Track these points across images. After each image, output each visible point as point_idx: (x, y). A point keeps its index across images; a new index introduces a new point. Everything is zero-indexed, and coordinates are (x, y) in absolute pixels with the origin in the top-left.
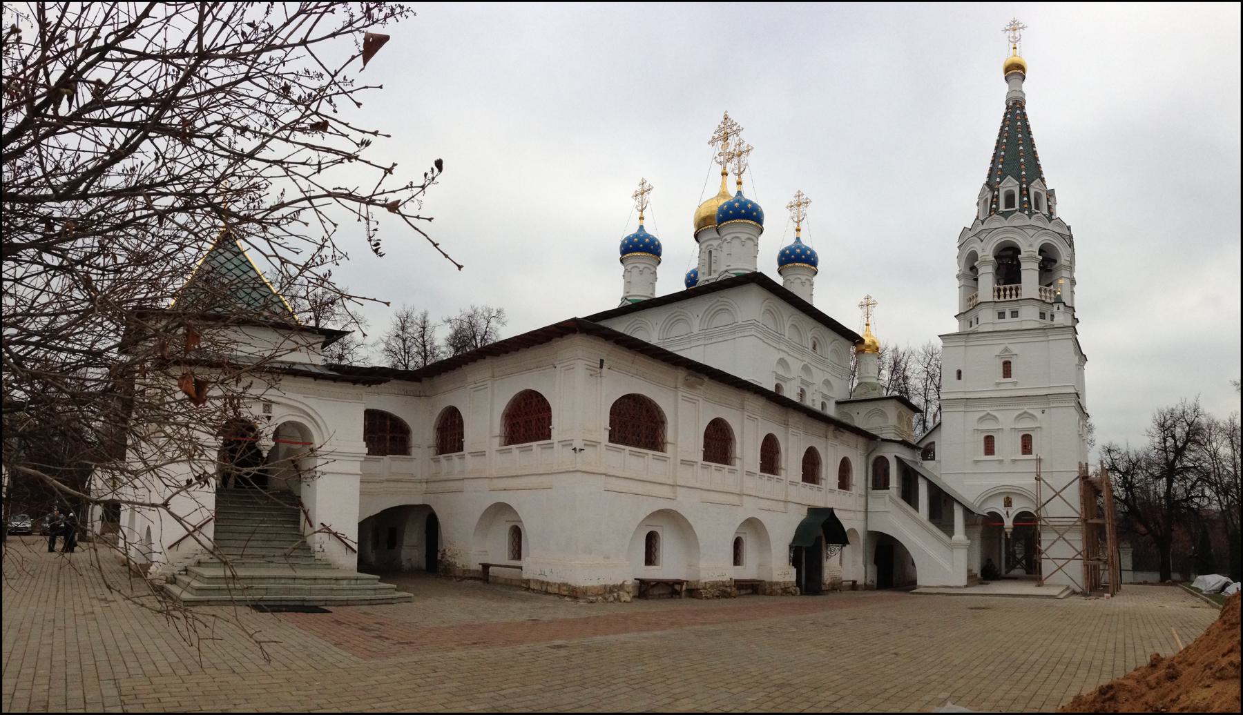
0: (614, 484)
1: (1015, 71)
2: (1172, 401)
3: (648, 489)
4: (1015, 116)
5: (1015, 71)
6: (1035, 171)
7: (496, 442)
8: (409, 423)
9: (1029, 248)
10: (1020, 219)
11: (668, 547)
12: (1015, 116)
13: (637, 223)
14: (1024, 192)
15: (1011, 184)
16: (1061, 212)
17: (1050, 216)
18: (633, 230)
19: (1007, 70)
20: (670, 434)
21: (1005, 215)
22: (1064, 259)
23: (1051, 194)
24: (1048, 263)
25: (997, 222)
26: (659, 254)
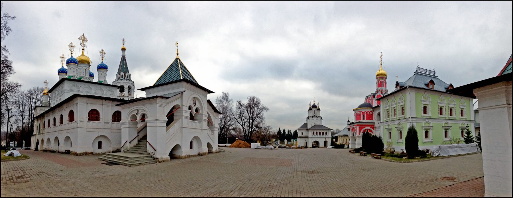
0: (88, 130)
1: (123, 50)
2: (252, 95)
3: (99, 130)
4: (124, 58)
5: (123, 50)
6: (127, 71)
7: (68, 122)
8: (68, 113)
9: (126, 87)
10: (124, 81)
11: (195, 145)
12: (124, 58)
13: (101, 61)
14: (125, 76)
15: (122, 73)
16: (132, 79)
17: (130, 80)
18: (100, 63)
19: (122, 49)
20: (101, 117)
21: (122, 80)
22: (132, 88)
23: (130, 74)
24: (129, 88)
25: (120, 81)
26: (107, 69)
